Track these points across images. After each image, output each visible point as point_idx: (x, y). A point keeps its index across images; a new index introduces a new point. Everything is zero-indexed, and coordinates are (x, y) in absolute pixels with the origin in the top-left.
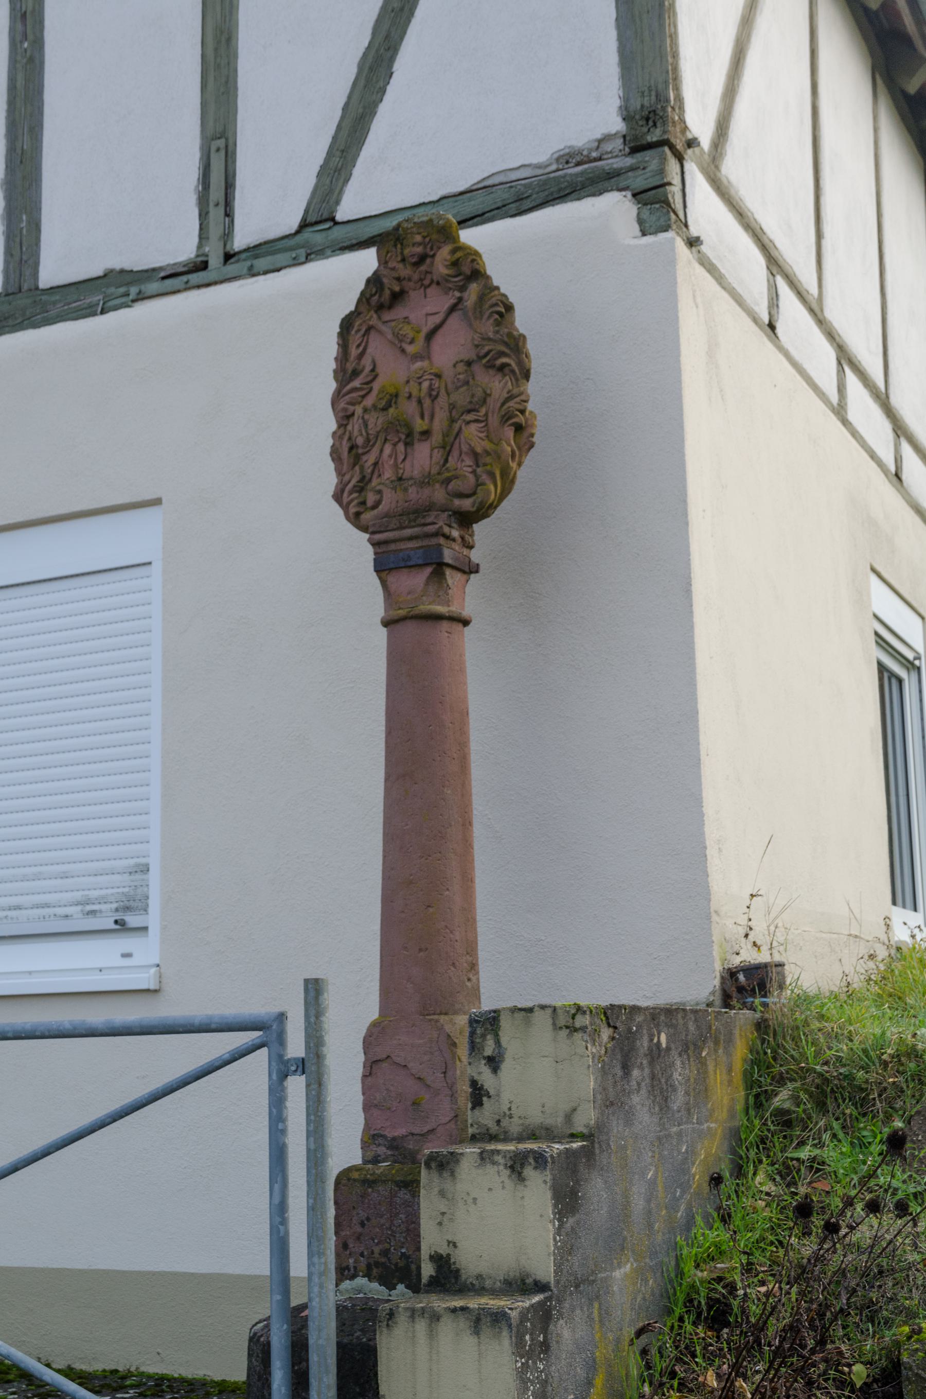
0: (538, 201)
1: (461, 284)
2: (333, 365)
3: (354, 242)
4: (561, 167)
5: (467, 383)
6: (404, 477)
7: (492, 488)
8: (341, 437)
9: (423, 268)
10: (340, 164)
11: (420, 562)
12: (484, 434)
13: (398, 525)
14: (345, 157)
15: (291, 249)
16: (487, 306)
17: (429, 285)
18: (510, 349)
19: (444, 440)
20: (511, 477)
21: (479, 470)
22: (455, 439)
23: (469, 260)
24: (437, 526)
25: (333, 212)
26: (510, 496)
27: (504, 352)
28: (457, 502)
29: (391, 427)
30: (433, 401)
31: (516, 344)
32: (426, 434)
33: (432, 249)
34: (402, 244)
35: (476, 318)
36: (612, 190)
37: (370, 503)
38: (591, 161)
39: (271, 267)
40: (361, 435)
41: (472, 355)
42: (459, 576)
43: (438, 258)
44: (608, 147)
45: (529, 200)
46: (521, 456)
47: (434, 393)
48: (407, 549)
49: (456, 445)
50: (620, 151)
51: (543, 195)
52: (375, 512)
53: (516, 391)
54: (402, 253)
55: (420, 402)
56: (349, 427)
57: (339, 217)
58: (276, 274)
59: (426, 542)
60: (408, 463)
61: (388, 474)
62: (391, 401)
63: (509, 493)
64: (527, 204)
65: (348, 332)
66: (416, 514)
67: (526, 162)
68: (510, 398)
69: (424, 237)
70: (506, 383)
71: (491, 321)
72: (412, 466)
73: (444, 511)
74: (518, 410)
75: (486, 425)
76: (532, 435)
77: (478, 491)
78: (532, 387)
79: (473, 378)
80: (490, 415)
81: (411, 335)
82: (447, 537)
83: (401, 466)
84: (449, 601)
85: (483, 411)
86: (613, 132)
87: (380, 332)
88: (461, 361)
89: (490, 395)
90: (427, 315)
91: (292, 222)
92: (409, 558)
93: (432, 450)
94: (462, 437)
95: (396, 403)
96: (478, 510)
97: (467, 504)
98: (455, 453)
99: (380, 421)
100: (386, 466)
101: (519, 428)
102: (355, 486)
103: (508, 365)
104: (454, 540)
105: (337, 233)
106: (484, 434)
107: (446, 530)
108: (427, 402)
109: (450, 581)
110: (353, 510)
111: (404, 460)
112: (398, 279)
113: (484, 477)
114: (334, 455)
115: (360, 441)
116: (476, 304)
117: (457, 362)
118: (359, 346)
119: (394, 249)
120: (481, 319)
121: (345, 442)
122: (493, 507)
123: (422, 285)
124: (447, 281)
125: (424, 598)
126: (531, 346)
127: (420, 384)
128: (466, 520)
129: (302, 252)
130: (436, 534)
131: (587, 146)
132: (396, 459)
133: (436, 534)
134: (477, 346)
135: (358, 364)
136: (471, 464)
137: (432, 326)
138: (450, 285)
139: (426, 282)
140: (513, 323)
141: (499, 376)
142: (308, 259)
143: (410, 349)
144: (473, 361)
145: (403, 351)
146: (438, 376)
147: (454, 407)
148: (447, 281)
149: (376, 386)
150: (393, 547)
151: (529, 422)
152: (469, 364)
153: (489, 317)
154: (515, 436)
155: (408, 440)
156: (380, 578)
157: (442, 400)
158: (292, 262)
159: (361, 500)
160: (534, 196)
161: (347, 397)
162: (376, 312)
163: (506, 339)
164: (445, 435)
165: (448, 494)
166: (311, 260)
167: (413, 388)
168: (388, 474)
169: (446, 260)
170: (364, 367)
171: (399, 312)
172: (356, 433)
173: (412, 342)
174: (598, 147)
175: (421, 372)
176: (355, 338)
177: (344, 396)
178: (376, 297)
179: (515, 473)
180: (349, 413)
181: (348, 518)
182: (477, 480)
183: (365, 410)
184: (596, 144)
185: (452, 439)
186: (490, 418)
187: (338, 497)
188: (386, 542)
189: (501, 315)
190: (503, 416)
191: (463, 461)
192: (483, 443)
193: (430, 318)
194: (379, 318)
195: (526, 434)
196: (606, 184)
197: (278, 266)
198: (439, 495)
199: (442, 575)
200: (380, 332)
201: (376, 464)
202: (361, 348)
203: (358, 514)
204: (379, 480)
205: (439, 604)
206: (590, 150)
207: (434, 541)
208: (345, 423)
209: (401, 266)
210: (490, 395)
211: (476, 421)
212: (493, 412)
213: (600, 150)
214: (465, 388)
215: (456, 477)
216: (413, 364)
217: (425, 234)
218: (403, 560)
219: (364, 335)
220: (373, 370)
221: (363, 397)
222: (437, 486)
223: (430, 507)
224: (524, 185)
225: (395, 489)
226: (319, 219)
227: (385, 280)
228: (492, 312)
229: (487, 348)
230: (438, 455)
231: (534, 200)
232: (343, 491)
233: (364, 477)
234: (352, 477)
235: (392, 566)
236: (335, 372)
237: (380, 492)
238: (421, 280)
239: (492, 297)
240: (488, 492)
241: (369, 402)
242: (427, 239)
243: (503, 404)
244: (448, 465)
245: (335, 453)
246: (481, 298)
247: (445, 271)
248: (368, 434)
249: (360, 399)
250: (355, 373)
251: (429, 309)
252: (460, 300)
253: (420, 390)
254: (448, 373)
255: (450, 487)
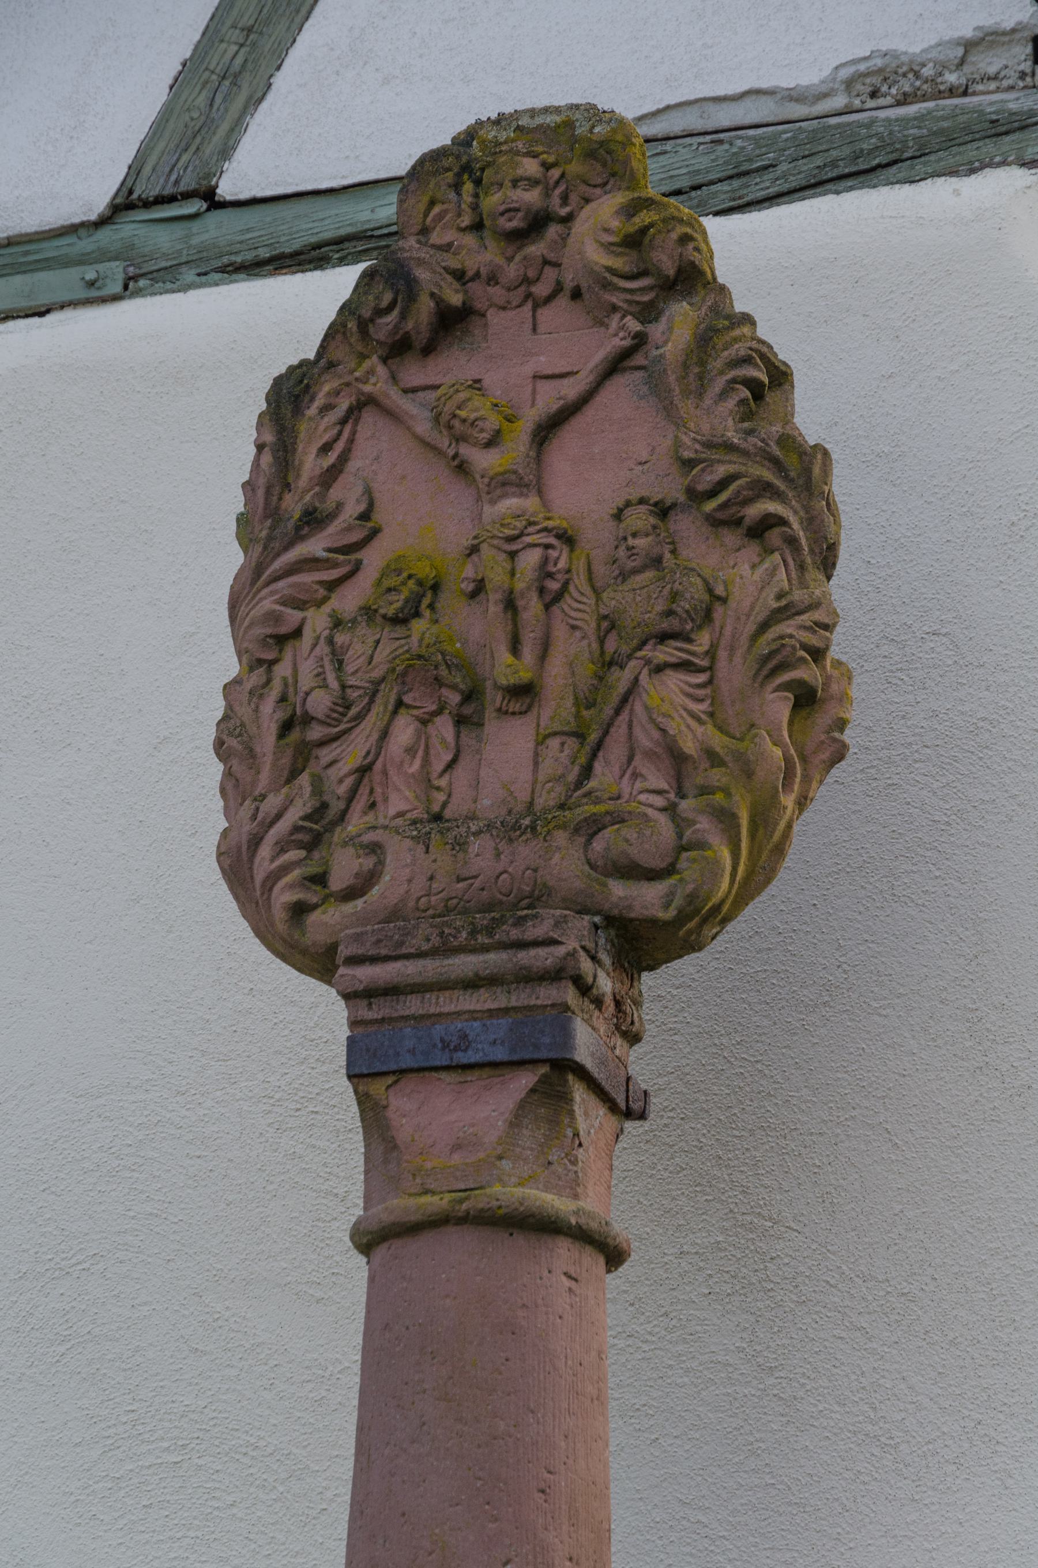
0: (794, 182)
1: (646, 298)
2: (237, 503)
3: (264, 253)
4: (857, 102)
5: (657, 562)
6: (448, 813)
7: (726, 855)
8: (257, 694)
9: (536, 249)
10: (239, 61)
11: (500, 1054)
12: (704, 706)
13: (436, 940)
14: (254, 44)
15: (82, 260)
16: (719, 364)
17: (549, 299)
18: (787, 479)
19: (577, 715)
20: (777, 836)
21: (686, 806)
22: (618, 712)
23: (674, 236)
24: (561, 951)
25: (209, 176)
26: (772, 889)
27: (767, 491)
28: (618, 889)
29: (421, 670)
30: (547, 607)
31: (803, 470)
32: (524, 693)
33: (565, 199)
34: (478, 182)
35: (686, 393)
36: (1004, 163)
37: (338, 881)
38: (939, 95)
39: (23, 303)
40: (325, 686)
41: (673, 490)
42: (600, 1111)
43: (582, 226)
44: (990, 63)
45: (769, 176)
46: (807, 779)
47: (554, 586)
48: (458, 1013)
49: (620, 731)
50: (1023, 75)
51: (807, 166)
52: (349, 908)
53: (798, 596)
54: (475, 207)
55: (510, 604)
56: (283, 670)
57: (227, 189)
58: (36, 320)
59: (520, 998)
60: (462, 774)
61: (400, 799)
62: (420, 597)
63: (768, 881)
64: (764, 185)
65: (298, 411)
66: (500, 914)
67: (764, 85)
68: (784, 612)
69: (547, 166)
70: (773, 572)
71: (731, 403)
72: (476, 784)
73: (583, 911)
74: (805, 647)
75: (710, 682)
76: (841, 724)
77: (682, 864)
78: (843, 589)
79: (673, 552)
80: (722, 654)
81: (494, 421)
82: (584, 989)
83: (443, 782)
84: (577, 1182)
85: (703, 640)
86: (1009, 24)
87: (392, 415)
88: (642, 501)
89: (724, 600)
90: (537, 377)
91: (97, 194)
92: (464, 1041)
93: (541, 741)
94: (638, 708)
95: (431, 606)
96: (682, 918)
97: (647, 899)
98: (615, 750)
99: (383, 654)
100: (395, 777)
101: (805, 699)
102: (296, 829)
103: (783, 522)
104: (598, 1002)
105: (217, 229)
106: (704, 706)
107: (586, 965)
108: (532, 608)
109: (582, 1125)
110: (284, 896)
111: (450, 766)
112: (459, 275)
113: (704, 824)
114: (233, 742)
115: (320, 703)
116: (688, 354)
117: (628, 504)
118: (326, 448)
119: (452, 195)
120: (700, 396)
121: (268, 706)
122: (719, 916)
123: (528, 296)
124: (606, 285)
125: (506, 1164)
126: (845, 486)
127: (513, 555)
128: (641, 946)
129: (115, 272)
130: (554, 975)
131: (933, 54)
132: (426, 762)
133: (554, 975)
134: (688, 464)
135: (322, 496)
136: (664, 786)
137: (555, 407)
138: (615, 299)
139: (541, 290)
140: (787, 418)
141: (752, 551)
142: (129, 288)
143: (486, 461)
144: (674, 505)
145: (461, 468)
146: (567, 539)
147: (613, 627)
148: (606, 285)
149: (374, 559)
150: (413, 1005)
151: (834, 688)
152: (663, 511)
153: (723, 395)
154: (791, 723)
155: (467, 710)
156: (363, 1100)
157: (580, 607)
158: (83, 294)
159: (313, 869)
160: (784, 167)
161: (281, 584)
162: (384, 360)
163: (776, 451)
164: (587, 702)
165: (592, 866)
166: (139, 293)
167: (493, 566)
168: (400, 799)
169: (606, 230)
170: (340, 506)
171: (452, 367)
172: (306, 681)
173: (491, 443)
174: (962, 62)
175: (520, 524)
176: (315, 428)
177: (268, 584)
178: (392, 318)
179: (789, 826)
180: (283, 630)
181: (264, 933)
182: (680, 836)
183: (337, 623)
184: (960, 51)
185: (608, 711)
186: (722, 664)
187: (236, 864)
188: (392, 991)
189: (757, 391)
190: (766, 659)
191: (635, 776)
192: (700, 730)
193: (544, 386)
194: (394, 378)
195: (823, 719)
196: (989, 148)
197: (43, 300)
198: (565, 863)
199: (564, 1098)
200: (392, 415)
201: (364, 771)
202: (332, 457)
203: (299, 911)
204: (370, 818)
205: (547, 1189)
206: (942, 67)
207: (546, 994)
208: (270, 656)
209: (470, 240)
210: (724, 600)
211: (684, 666)
212: (732, 649)
213: (967, 69)
214: (650, 574)
215: (619, 819)
216: (493, 502)
217: (551, 159)
218: (445, 1045)
219: (343, 422)
220: (365, 516)
221: (332, 586)
222: (561, 837)
223: (536, 898)
224: (755, 139)
225: (425, 841)
226: (168, 191)
227: (422, 274)
228: (734, 381)
229: (721, 471)
230: (559, 756)
231: (784, 176)
232: (255, 841)
233: (324, 806)
234: (289, 802)
235: (407, 1062)
236: (243, 521)
237: (375, 849)
238: (526, 281)
239: (736, 340)
240: (714, 869)
241: (349, 600)
242: (555, 173)
243: (764, 627)
244: (592, 784)
245: (232, 742)
246: (705, 341)
247: (600, 259)
248: (343, 687)
249: (322, 592)
250: (313, 520)
251: (543, 363)
252: (640, 340)
253: (513, 573)
254: (597, 536)
255: (598, 845)
